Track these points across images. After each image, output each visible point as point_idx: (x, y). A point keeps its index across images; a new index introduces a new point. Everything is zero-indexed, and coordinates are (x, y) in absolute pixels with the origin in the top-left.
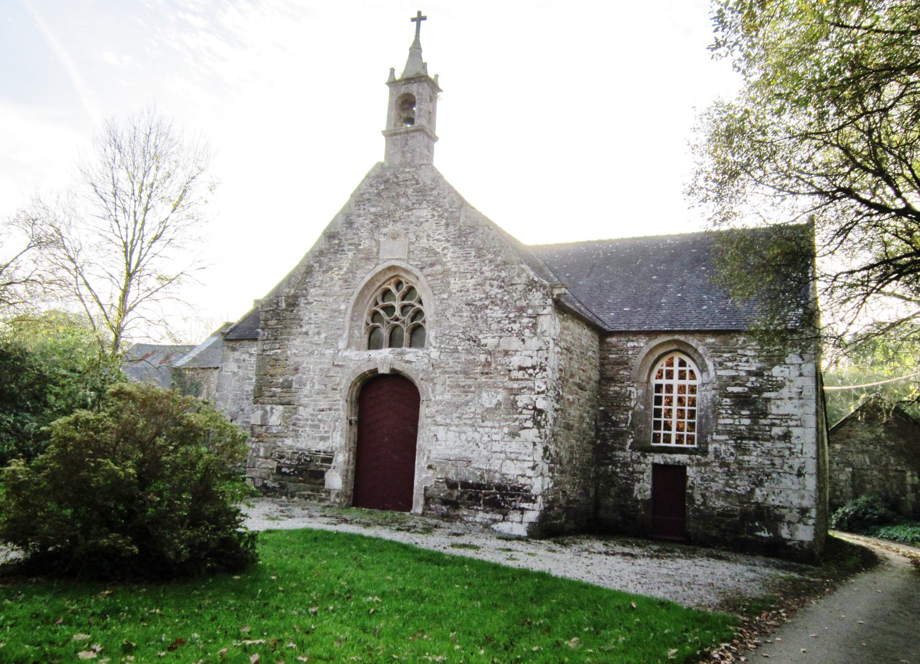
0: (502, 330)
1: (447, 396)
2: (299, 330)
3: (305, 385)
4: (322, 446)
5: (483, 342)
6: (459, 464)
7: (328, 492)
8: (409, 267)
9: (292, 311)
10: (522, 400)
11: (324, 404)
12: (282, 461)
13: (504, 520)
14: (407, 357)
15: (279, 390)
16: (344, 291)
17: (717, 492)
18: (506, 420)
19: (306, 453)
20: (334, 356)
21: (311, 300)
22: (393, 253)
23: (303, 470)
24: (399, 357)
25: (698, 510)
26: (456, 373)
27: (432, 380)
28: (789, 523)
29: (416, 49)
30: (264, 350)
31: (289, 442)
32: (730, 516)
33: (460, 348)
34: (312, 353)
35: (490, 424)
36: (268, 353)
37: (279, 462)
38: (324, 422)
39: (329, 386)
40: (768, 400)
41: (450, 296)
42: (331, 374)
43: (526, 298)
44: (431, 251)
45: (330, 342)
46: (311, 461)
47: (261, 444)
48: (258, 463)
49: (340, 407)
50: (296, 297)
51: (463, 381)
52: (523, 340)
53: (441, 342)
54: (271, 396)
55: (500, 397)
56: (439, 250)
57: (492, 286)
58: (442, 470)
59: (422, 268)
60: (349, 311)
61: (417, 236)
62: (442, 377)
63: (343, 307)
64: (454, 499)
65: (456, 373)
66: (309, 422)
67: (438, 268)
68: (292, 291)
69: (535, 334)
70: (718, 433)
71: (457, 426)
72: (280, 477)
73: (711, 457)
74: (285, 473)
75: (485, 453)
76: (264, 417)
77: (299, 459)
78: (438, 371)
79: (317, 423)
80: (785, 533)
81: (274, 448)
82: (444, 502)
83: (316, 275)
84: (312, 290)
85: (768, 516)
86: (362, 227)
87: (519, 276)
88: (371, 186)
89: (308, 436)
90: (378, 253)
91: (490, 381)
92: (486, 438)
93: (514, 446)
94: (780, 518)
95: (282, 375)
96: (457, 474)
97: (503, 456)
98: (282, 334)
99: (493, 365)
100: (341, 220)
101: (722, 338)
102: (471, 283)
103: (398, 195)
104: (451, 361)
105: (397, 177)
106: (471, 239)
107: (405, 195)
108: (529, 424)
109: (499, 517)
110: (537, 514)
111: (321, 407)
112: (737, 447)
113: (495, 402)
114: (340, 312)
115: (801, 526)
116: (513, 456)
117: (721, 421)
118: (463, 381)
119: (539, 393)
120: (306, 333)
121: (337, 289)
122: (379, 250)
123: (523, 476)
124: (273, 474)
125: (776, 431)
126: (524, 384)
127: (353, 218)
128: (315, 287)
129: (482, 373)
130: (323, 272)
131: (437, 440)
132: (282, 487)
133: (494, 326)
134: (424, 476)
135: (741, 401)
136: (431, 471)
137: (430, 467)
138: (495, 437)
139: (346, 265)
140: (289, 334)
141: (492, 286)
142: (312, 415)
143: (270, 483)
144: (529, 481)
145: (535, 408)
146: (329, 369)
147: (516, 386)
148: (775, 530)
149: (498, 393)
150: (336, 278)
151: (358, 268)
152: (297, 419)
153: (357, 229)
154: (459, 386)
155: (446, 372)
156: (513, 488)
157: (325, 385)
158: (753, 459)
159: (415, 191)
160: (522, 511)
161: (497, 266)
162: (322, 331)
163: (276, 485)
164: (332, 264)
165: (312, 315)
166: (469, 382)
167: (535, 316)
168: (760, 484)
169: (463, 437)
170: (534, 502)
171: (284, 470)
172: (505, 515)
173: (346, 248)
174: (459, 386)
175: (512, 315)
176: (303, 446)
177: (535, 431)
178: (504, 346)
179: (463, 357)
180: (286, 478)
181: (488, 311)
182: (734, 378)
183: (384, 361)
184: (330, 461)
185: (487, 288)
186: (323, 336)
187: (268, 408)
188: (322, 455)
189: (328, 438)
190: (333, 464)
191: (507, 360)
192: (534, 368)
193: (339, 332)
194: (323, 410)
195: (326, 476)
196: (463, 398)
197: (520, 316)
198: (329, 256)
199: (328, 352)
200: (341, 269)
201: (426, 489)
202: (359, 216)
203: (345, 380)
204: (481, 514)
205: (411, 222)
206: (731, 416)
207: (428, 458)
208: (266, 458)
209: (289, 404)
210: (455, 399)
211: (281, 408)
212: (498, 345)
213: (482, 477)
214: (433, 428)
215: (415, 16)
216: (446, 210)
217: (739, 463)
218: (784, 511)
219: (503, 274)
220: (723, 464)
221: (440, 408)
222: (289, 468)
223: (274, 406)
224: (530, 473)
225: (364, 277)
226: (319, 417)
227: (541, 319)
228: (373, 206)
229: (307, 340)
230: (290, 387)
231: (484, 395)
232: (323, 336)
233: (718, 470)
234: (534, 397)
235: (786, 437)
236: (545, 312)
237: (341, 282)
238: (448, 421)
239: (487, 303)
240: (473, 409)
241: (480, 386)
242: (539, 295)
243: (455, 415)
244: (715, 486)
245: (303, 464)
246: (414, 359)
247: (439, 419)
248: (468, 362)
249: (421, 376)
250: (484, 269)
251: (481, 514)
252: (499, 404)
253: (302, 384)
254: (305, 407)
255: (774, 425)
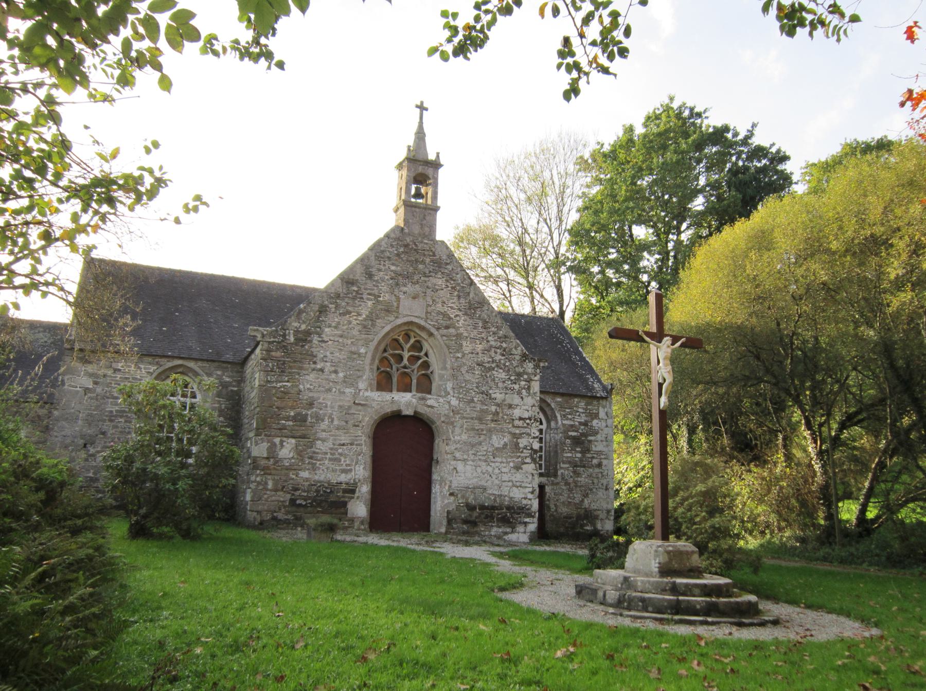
0: (506, 388)
1: (464, 437)
2: (313, 366)
3: (323, 420)
4: (343, 478)
5: (493, 396)
6: (477, 491)
7: (352, 520)
8: (428, 326)
9: (303, 346)
10: (523, 442)
11: (344, 439)
12: (297, 493)
13: (512, 532)
14: (429, 402)
15: (291, 423)
16: (363, 336)
17: (563, 503)
18: (512, 457)
19: (326, 485)
20: (355, 395)
21: (326, 339)
22: (411, 309)
23: (322, 501)
24: (422, 402)
25: (552, 515)
26: (472, 418)
27: (452, 423)
28: (602, 519)
29: (420, 135)
30: (268, 382)
31: (305, 474)
32: (571, 518)
33: (476, 399)
34: (329, 390)
35: (499, 460)
36: (274, 385)
37: (293, 495)
38: (345, 456)
39: (351, 422)
40: (590, 441)
41: (463, 356)
42: (352, 411)
43: (522, 367)
44: (445, 315)
45: (349, 381)
46: (331, 492)
47: (269, 477)
48: (266, 496)
49: (362, 442)
50: (308, 333)
51: (478, 426)
52: (522, 398)
53: (459, 393)
54: (280, 429)
55: (506, 440)
56: (452, 316)
57: (496, 353)
58: (463, 497)
59: (438, 329)
60: (369, 356)
61: (434, 301)
62: (461, 421)
63: (362, 351)
64: (473, 518)
65: (472, 418)
66: (329, 456)
67: (452, 331)
68: (303, 327)
69: (529, 393)
70: (564, 463)
71: (473, 461)
72: (294, 509)
73: (559, 479)
74: (300, 505)
75: (497, 482)
76: (272, 449)
77: (317, 491)
78: (458, 416)
79: (337, 456)
80: (599, 526)
81: (286, 481)
82: (465, 522)
83: (331, 316)
84: (327, 330)
85: (590, 516)
86: (383, 281)
87: (516, 348)
88: (392, 246)
89: (327, 469)
90: (398, 307)
91: (498, 427)
92: (497, 471)
93: (518, 476)
94: (596, 517)
95: (292, 408)
96: (475, 499)
97: (510, 484)
98: (291, 367)
99: (501, 415)
100: (360, 270)
101: (566, 398)
102: (479, 348)
103: (417, 261)
104: (468, 409)
105: (416, 245)
106: (478, 313)
107: (423, 262)
108: (528, 460)
109: (509, 530)
110: (535, 525)
111: (342, 442)
112: (574, 472)
113: (502, 443)
114: (359, 354)
115: (607, 521)
116: (518, 484)
117: (565, 455)
118: (478, 426)
119: (534, 438)
120: (322, 370)
121: (355, 332)
122: (398, 305)
123: (525, 498)
124: (285, 507)
125: (595, 461)
126: (524, 430)
127: (374, 270)
128: (330, 326)
129: (492, 421)
130: (340, 314)
131: (457, 472)
132: (297, 518)
133: (500, 385)
134: (446, 501)
135: (577, 441)
136: (452, 498)
137: (452, 494)
138: (504, 470)
139: (365, 313)
140: (301, 368)
141: (496, 353)
142: (331, 449)
143: (280, 516)
144: (529, 502)
145: (532, 449)
146: (349, 407)
147: (517, 432)
148: (594, 525)
149: (504, 436)
150: (355, 322)
151: (378, 317)
152: (314, 452)
153: (377, 281)
154: (473, 429)
155: (464, 418)
156: (519, 508)
157: (347, 422)
158: (583, 480)
159: (432, 261)
160: (526, 524)
161: (499, 338)
162: (339, 370)
163: (290, 517)
164: (350, 309)
165: (328, 354)
166: (482, 427)
167: (529, 381)
168: (586, 496)
169: (479, 470)
170: (533, 517)
171: (298, 502)
172: (513, 528)
173: (365, 296)
174: (473, 429)
175: (513, 378)
176: (322, 478)
177: (533, 466)
178: (508, 401)
179: (479, 407)
180: (302, 509)
181: (494, 372)
182: (572, 426)
183: (408, 404)
184: (353, 492)
185: (493, 354)
186: (341, 375)
187: (277, 440)
188: (344, 486)
189: (351, 470)
190: (356, 495)
191: (510, 412)
192: (530, 419)
193: (359, 373)
194: (343, 445)
195: (349, 506)
196: (476, 440)
197: (519, 380)
198: (346, 300)
199: (347, 390)
200: (359, 314)
201: (448, 512)
202: (380, 270)
203: (368, 419)
204: (495, 529)
205: (428, 287)
206: (570, 452)
207: (450, 487)
208: (276, 490)
209: (303, 437)
210: (470, 440)
211: (293, 441)
212: (504, 400)
213: (495, 500)
214: (453, 463)
215: (419, 104)
216: (459, 284)
217: (575, 482)
218: (599, 512)
219: (504, 345)
220: (567, 484)
221: (458, 446)
222: (305, 500)
223: (284, 439)
224: (530, 496)
225: (385, 327)
226: (340, 451)
227: (533, 383)
228: (393, 264)
229: (323, 377)
230: (305, 421)
231: (494, 437)
232: (341, 375)
233: (564, 487)
234: (531, 441)
235: (600, 465)
236: (536, 378)
237: (360, 327)
238: (465, 457)
239: (493, 365)
240: (485, 448)
241: (490, 431)
242: (531, 365)
243: (471, 452)
244: (562, 499)
245: (322, 495)
246: (436, 405)
247: (458, 455)
248: (482, 411)
249: (443, 419)
250: (490, 338)
251: (495, 529)
252: (505, 445)
253: (319, 419)
254: (323, 440)
255: (593, 458)
